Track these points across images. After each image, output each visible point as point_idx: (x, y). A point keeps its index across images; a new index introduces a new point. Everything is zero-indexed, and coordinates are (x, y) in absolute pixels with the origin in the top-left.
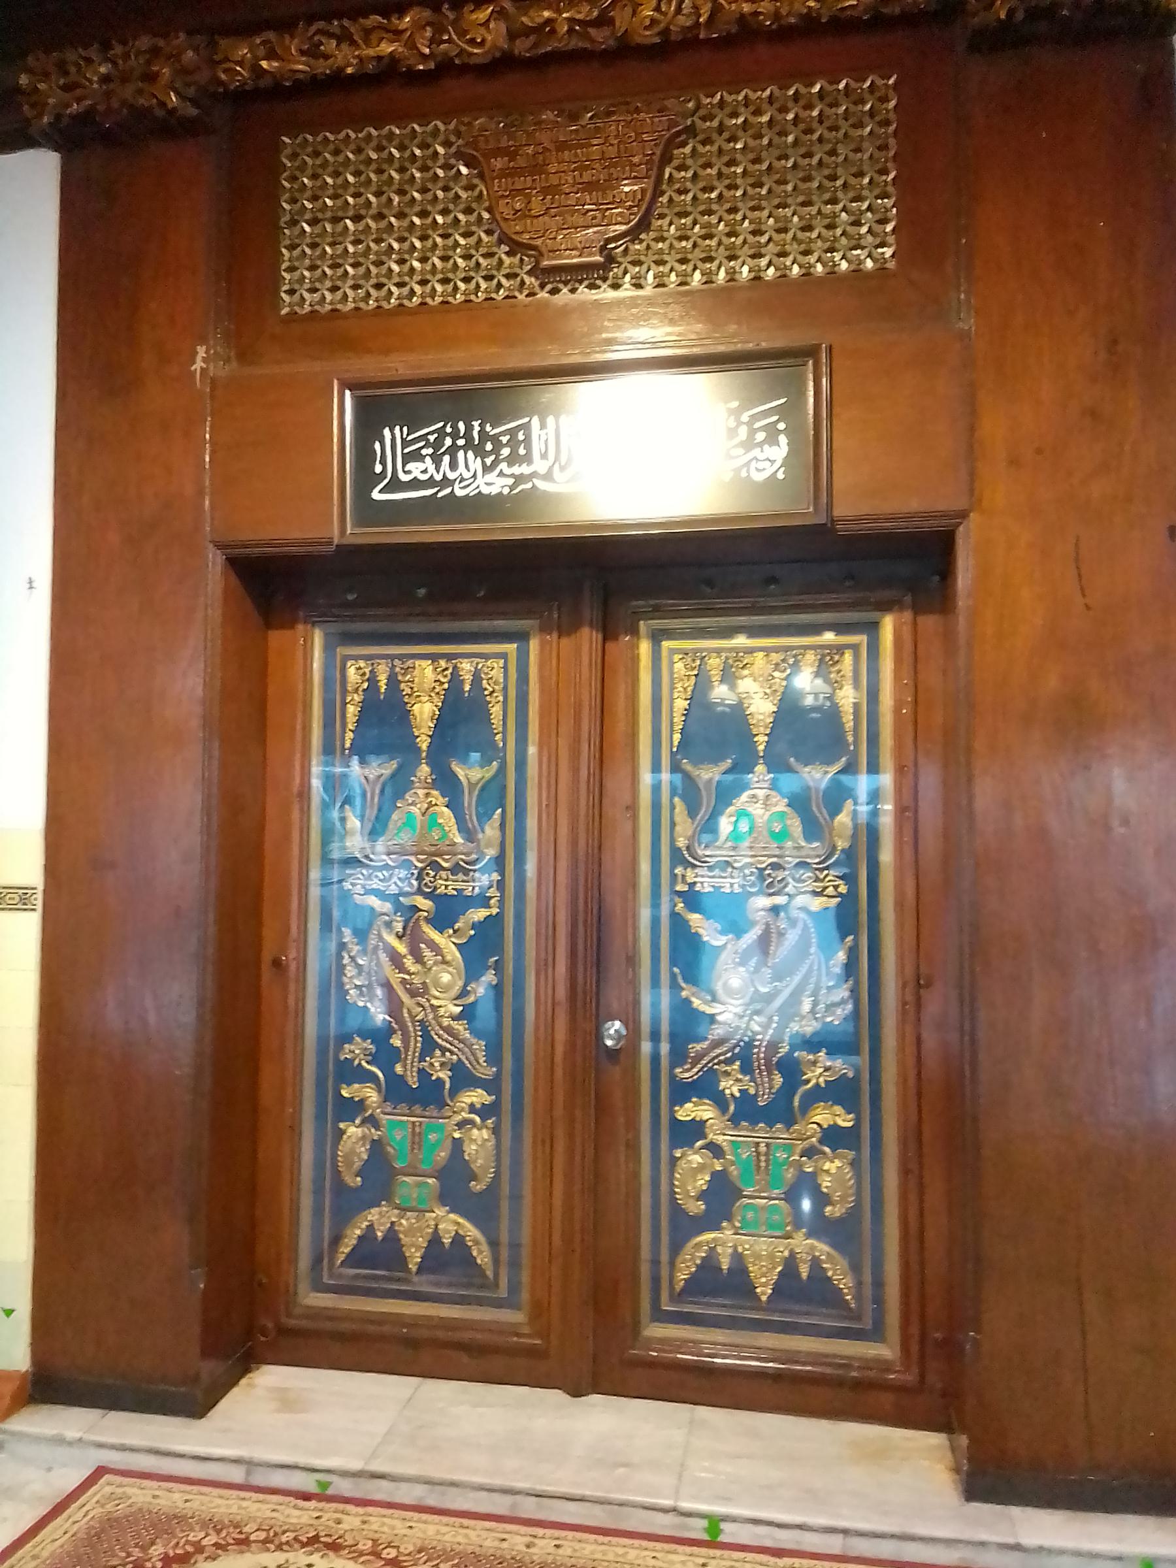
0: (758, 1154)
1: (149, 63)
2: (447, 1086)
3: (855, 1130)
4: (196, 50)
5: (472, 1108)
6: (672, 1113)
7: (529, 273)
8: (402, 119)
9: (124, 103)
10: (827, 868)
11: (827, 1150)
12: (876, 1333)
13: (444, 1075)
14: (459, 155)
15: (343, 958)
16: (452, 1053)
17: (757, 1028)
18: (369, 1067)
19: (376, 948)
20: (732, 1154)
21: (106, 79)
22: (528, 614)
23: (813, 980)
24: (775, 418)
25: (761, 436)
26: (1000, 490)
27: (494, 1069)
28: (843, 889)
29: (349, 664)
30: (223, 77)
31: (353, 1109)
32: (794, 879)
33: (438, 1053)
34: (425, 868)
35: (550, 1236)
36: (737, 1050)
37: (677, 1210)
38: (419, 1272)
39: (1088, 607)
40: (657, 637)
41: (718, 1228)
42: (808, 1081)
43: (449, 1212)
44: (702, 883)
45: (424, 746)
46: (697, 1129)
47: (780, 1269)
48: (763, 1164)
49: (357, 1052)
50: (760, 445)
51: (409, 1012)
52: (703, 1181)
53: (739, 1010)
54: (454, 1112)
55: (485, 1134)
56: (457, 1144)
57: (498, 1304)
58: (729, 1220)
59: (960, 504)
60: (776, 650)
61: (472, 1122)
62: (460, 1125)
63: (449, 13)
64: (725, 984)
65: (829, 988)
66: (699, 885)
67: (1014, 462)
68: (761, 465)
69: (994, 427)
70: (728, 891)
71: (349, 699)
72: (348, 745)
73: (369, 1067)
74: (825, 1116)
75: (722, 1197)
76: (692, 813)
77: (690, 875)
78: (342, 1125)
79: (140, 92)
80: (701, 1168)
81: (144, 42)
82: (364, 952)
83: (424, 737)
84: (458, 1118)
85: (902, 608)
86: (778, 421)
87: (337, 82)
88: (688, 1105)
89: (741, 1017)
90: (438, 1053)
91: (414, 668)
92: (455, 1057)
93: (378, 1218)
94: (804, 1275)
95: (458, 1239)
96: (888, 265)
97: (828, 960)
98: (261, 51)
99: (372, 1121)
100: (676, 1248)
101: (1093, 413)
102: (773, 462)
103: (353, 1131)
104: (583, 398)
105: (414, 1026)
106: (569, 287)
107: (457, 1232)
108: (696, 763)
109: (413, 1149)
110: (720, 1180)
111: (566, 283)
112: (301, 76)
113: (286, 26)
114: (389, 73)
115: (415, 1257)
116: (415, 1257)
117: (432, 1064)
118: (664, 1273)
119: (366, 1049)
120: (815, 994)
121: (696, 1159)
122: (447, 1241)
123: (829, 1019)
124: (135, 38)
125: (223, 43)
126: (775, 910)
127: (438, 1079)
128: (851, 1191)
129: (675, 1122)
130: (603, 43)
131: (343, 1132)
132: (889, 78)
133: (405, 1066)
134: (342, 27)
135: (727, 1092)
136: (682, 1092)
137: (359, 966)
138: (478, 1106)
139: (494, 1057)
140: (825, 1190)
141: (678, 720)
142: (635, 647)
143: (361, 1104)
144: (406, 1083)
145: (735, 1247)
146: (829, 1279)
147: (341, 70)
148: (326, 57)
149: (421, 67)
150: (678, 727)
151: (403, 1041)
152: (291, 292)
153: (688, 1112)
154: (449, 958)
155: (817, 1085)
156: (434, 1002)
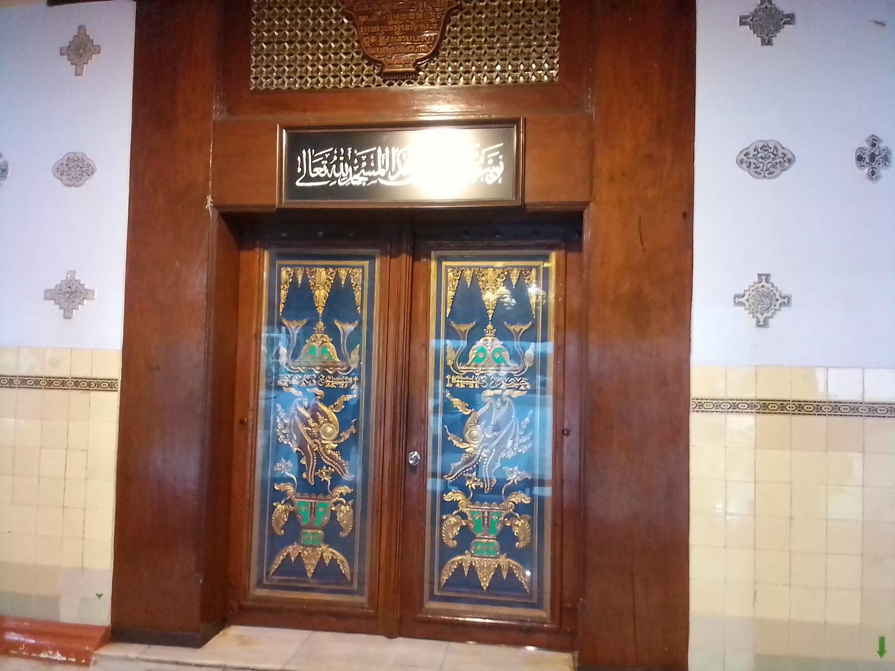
5: (341, 495)
22: (375, 246)
39: (644, 250)
41: (463, 553)
46: (455, 504)
56: (334, 514)
58: (469, 550)
61: (341, 502)
62: (335, 504)
67: (611, 179)
69: (602, 162)
75: (466, 538)
77: (454, 379)
80: (456, 524)
84: (334, 500)
95: (333, 560)
108: (458, 323)
110: (293, 515)
111: (396, 81)
115: (310, 570)
116: (310, 570)
120: (514, 437)
121: (453, 520)
122: (327, 562)
129: (443, 501)
145: (471, 563)
152: (256, 78)
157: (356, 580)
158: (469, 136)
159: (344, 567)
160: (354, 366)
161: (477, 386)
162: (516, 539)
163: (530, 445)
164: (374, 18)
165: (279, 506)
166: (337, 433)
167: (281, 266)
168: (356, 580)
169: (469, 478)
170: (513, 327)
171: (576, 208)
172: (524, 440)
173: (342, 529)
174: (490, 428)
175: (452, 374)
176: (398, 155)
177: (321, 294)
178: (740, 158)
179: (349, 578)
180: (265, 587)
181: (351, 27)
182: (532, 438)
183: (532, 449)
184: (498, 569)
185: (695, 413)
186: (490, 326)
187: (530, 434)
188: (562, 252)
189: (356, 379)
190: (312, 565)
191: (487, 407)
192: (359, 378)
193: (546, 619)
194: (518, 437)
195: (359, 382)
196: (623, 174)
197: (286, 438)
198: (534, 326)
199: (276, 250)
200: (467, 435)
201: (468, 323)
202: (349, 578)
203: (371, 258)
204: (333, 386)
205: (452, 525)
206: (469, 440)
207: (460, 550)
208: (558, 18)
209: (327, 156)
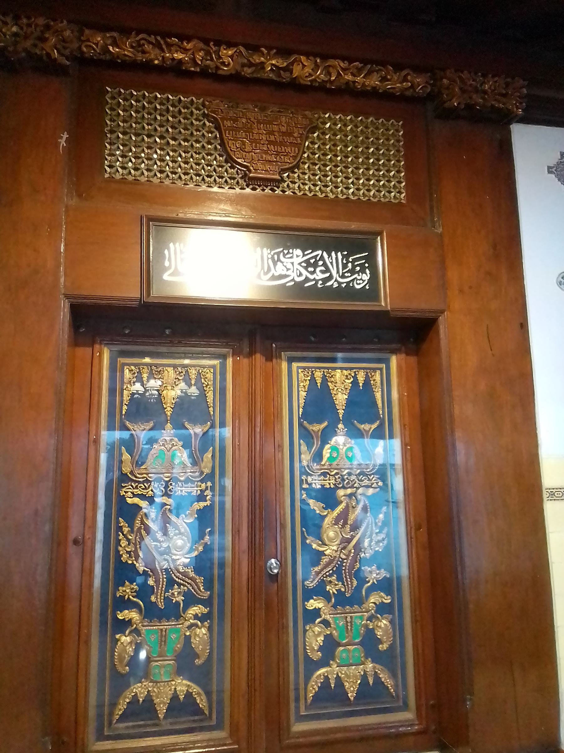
0: (347, 622)
1: (42, 32)
2: (182, 606)
3: (391, 605)
4: (72, 32)
5: (196, 617)
6: (304, 606)
7: (241, 178)
8: (152, 88)
9: (25, 50)
10: (373, 474)
11: (379, 616)
12: (405, 707)
13: (180, 598)
14: (204, 115)
15: (119, 535)
16: (184, 586)
17: (344, 557)
18: (135, 599)
19: (140, 528)
20: (334, 625)
21: (15, 35)
22: (227, 346)
23: (370, 529)
24: (364, 261)
25: (358, 269)
26: (457, 303)
27: (209, 593)
28: (380, 484)
29: (125, 367)
30: (85, 49)
31: (123, 626)
32: (358, 480)
33: (176, 586)
34: (169, 481)
35: (77, 679)
36: (335, 569)
37: (307, 657)
38: (164, 718)
39: (493, 355)
40: (291, 360)
41: (329, 665)
42: (369, 582)
43: (182, 680)
44: (315, 483)
45: (169, 414)
46: (317, 612)
47: (359, 681)
48: (349, 627)
49: (127, 591)
50: (358, 272)
51: (159, 563)
52: (321, 639)
53: (335, 548)
54: (186, 620)
55: (204, 631)
56: (188, 639)
57: (210, 728)
58: (334, 660)
59: (440, 307)
60: (346, 369)
61: (197, 626)
62: (189, 627)
63: (213, 47)
64: (328, 535)
65: (377, 533)
66: (314, 484)
67: (461, 291)
68: (358, 282)
69: (453, 274)
70: (328, 487)
71: (125, 387)
72: (124, 413)
73: (135, 599)
74: (374, 599)
75: (330, 646)
76: (309, 447)
77: (310, 479)
78: (117, 636)
79: (35, 46)
80: (319, 634)
81: (41, 21)
82: (132, 531)
83: (169, 409)
84: (187, 623)
85: (400, 353)
86: (365, 263)
87: (147, 67)
88: (312, 601)
89: (336, 551)
90: (176, 586)
91: (164, 371)
92: (185, 588)
93: (139, 690)
94: (371, 683)
95: (189, 695)
96: (402, 201)
97: (375, 519)
98: (109, 42)
99: (137, 632)
100: (307, 679)
101: (489, 273)
102: (364, 281)
103: (125, 639)
104: (193, 237)
105: (162, 573)
106: (261, 188)
107: (187, 690)
108: (310, 423)
109: (161, 645)
110: (329, 638)
111: (259, 186)
112: (127, 58)
113: (126, 32)
114: (178, 69)
115: (162, 710)
116: (162, 710)
117: (173, 594)
118: (302, 693)
119: (133, 589)
120: (370, 536)
121: (317, 629)
122: (182, 697)
123: (377, 549)
124: (36, 18)
125: (87, 32)
126: (350, 496)
127: (176, 601)
128: (390, 636)
129: (305, 610)
130: (285, 79)
131: (118, 640)
132: (326, 114)
133: (157, 597)
134: (156, 39)
135: (331, 591)
136: (309, 594)
137: (129, 540)
138: (200, 615)
139: (209, 585)
140: (379, 637)
141: (302, 401)
142: (280, 365)
143: (129, 622)
144: (158, 606)
145: (337, 674)
146: (383, 683)
147: (152, 60)
148: (144, 52)
149: (193, 69)
150: (302, 405)
151: (155, 582)
152: (110, 167)
153: (313, 604)
154: (183, 530)
155: (373, 583)
156: (174, 557)
157: (214, 716)
158: (246, 239)
159: (202, 700)
160: (207, 471)
161: (332, 486)
162: (380, 642)
163: (385, 542)
164: (240, 125)
165: (123, 638)
166: (189, 545)
167: (124, 365)
168: (214, 716)
169: (330, 582)
170: (363, 426)
171: (433, 315)
172: (380, 537)
173: (197, 656)
174: (348, 528)
175: (308, 474)
176: (270, 256)
177: (341, 398)
178: (559, 280)
179: (207, 712)
180: (108, 738)
181: (213, 129)
182: (388, 535)
183: (389, 544)
184: (364, 677)
185: (549, 502)
186: (340, 426)
187: (385, 531)
188: (403, 356)
189: (209, 484)
190: (164, 703)
191: (343, 506)
192: (213, 483)
193: (412, 720)
194: (374, 535)
195: (212, 489)
196: (470, 287)
197: (130, 556)
198: (381, 425)
199: (116, 348)
200: (325, 537)
201: (320, 422)
202: (207, 712)
203: (224, 357)
204: (184, 493)
205: (315, 638)
206: (327, 543)
207: (324, 662)
208: (402, 149)
209: (312, 261)
